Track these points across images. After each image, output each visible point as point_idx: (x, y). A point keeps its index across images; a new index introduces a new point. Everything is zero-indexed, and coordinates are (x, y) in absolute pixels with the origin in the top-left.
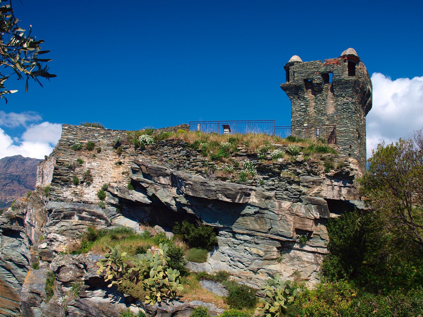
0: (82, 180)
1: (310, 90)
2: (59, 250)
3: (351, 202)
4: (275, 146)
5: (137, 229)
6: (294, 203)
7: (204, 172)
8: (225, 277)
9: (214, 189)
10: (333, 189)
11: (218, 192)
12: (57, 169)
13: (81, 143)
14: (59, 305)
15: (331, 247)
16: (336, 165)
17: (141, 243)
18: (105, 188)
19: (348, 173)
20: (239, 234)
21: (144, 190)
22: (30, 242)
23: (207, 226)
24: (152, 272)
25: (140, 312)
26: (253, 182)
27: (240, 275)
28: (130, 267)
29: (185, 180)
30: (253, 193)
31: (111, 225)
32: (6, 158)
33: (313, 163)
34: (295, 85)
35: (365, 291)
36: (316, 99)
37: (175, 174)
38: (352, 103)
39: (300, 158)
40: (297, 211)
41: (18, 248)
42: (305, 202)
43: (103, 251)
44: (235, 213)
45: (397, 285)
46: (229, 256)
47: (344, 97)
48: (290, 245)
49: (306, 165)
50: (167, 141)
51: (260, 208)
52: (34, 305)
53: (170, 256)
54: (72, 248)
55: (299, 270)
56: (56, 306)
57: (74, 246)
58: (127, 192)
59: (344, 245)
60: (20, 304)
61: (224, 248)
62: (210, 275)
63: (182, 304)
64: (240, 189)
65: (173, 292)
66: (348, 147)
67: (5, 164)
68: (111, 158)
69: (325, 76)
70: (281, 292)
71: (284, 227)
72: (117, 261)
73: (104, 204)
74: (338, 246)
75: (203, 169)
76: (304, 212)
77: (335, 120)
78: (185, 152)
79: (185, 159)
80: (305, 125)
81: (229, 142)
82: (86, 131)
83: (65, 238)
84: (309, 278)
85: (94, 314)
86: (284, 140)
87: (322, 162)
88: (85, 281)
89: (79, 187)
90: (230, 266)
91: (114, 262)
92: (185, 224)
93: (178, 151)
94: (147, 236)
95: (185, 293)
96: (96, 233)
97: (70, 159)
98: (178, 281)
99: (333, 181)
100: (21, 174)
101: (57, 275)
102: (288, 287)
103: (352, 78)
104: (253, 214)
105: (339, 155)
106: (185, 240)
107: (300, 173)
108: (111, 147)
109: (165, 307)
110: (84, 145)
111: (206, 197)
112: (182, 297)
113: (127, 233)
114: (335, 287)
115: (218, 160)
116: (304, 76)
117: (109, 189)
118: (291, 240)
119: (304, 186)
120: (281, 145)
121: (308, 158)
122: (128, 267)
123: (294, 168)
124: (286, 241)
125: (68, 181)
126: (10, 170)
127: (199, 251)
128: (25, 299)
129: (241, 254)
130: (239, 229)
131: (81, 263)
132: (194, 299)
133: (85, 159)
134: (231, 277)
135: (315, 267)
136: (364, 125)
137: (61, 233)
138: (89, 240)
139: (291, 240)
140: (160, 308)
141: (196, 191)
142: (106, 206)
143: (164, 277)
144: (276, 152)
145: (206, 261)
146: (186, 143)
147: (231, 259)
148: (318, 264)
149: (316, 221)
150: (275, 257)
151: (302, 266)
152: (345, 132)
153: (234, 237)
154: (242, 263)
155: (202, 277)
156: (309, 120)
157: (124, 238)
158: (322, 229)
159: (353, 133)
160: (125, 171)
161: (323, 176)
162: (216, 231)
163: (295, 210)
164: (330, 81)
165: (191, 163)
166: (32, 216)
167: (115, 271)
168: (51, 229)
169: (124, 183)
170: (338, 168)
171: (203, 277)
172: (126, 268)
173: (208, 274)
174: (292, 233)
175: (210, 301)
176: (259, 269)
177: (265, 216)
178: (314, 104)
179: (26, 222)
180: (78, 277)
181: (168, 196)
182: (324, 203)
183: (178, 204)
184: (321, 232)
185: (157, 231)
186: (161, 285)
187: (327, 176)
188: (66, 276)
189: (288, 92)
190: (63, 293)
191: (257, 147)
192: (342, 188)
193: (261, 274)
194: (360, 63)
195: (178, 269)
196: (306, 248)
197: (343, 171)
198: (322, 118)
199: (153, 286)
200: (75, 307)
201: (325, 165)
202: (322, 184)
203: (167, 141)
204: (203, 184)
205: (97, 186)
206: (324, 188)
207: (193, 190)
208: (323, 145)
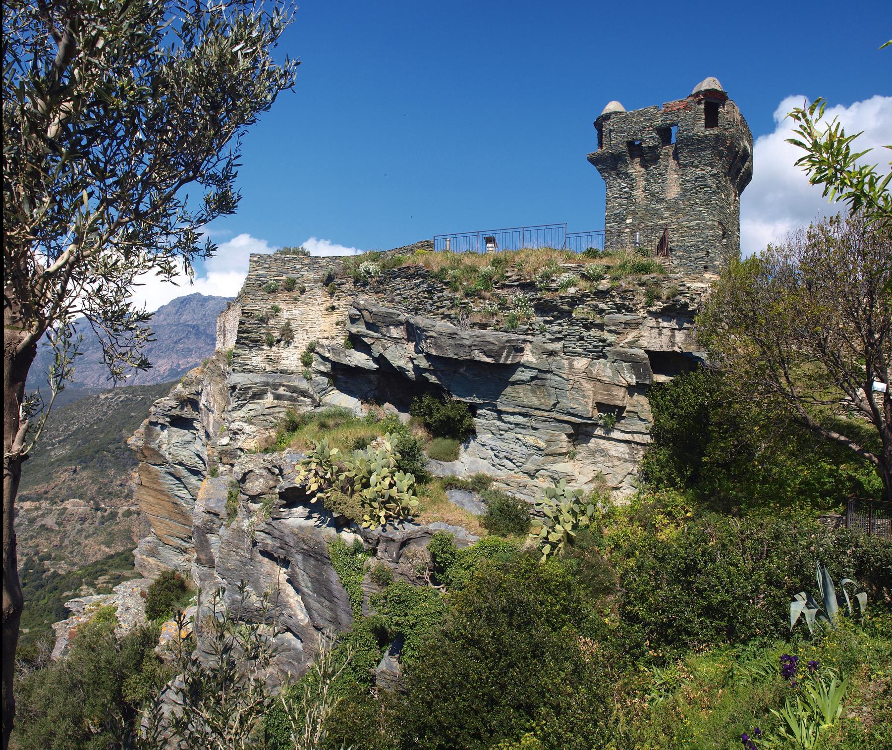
0: (279, 338)
1: (638, 160)
2: (246, 446)
3: (696, 354)
4: (563, 268)
5: (358, 409)
6: (594, 361)
7: (453, 316)
8: (484, 483)
9: (467, 342)
10: (660, 334)
11: (473, 348)
12: (244, 324)
13: (277, 281)
14: (243, 531)
15: (657, 433)
16: (665, 293)
17: (362, 433)
18: (312, 349)
19: (686, 305)
20: (508, 413)
21: (366, 349)
22: (208, 436)
23: (458, 402)
24: (373, 479)
25: (356, 540)
26: (528, 329)
27: (508, 482)
28: (343, 472)
29: (426, 331)
30: (528, 347)
31: (319, 405)
32: (179, 298)
33: (626, 291)
35: (708, 508)
36: (648, 174)
37: (411, 321)
38: (711, 176)
39: (604, 285)
40: (598, 373)
41: (191, 445)
42: (611, 358)
43: (307, 447)
44: (500, 380)
45: (766, 498)
46: (493, 450)
47: (697, 167)
48: (589, 429)
49: (614, 297)
50: (399, 269)
51: (540, 371)
52: (211, 531)
53: (402, 452)
54: (264, 443)
55: (604, 472)
56: (240, 532)
57: (266, 441)
58: (343, 352)
59: (677, 429)
60: (192, 529)
61: (484, 437)
62: (462, 482)
63: (416, 528)
64: (507, 342)
65: (404, 509)
66: (703, 253)
67: (176, 309)
68: (319, 300)
69: (664, 133)
70: (567, 509)
71: (577, 400)
72: (325, 461)
73: (309, 373)
74: (667, 431)
75: (453, 312)
76: (611, 374)
78: (425, 285)
79: (425, 298)
80: (628, 221)
81: (493, 265)
82: (283, 261)
83: (254, 428)
84: (620, 485)
85: (291, 544)
86: (580, 257)
87: (642, 290)
88: (279, 493)
89: (274, 349)
90: (494, 465)
91: (319, 464)
92: (426, 400)
93: (415, 284)
94: (372, 420)
95: (422, 510)
96: (298, 420)
97: (260, 307)
98: (411, 491)
99: (660, 320)
100: (200, 322)
101: (242, 485)
102: (577, 501)
103: (712, 132)
104: (529, 381)
105: (671, 275)
106: (427, 426)
107: (604, 311)
108: (320, 284)
109: (392, 533)
110: (281, 283)
111: (456, 357)
112: (417, 516)
113: (343, 416)
114: (659, 501)
115: (474, 296)
116: (628, 136)
117: (318, 349)
118: (589, 422)
119: (610, 331)
120: (573, 265)
121: (617, 283)
122: (341, 470)
123: (594, 302)
124: (582, 423)
125: (258, 341)
126: (184, 318)
127: (447, 442)
128: (198, 522)
129: (511, 446)
130: (507, 405)
131: (275, 467)
132: (435, 520)
133: (283, 306)
134: (495, 483)
135: (630, 467)
136: (737, 213)
137: (249, 421)
138: (288, 430)
139: (589, 422)
140: (383, 534)
141: (442, 348)
142: (313, 376)
143: (391, 486)
144: (565, 277)
145: (457, 459)
146: (427, 272)
147: (495, 455)
148: (635, 462)
149: (631, 390)
150: (564, 451)
151: (608, 464)
152: (699, 229)
153: (500, 419)
154: (511, 460)
155: (450, 484)
156: (634, 213)
157: (337, 425)
158: (642, 402)
159: (712, 229)
160: (340, 320)
161: (642, 313)
162: (473, 409)
163: (595, 373)
164: (673, 140)
165: (435, 302)
166: (211, 396)
167: (322, 477)
168: (235, 415)
169: (339, 338)
170: (668, 298)
171: (451, 484)
172: (337, 472)
173: (458, 480)
174: (591, 409)
175: (459, 523)
176: (538, 471)
177: (548, 383)
178: (644, 183)
179: (201, 405)
180: (271, 489)
181: (402, 356)
182: (644, 359)
183: (416, 368)
184: (640, 408)
185: (387, 412)
186: (386, 498)
187: (649, 312)
188: (255, 486)
189: (600, 166)
190: (250, 513)
191: (535, 271)
192: (676, 332)
193: (541, 479)
194: (728, 102)
195: (413, 472)
196: (616, 434)
197: (676, 303)
198: (659, 206)
199: (375, 500)
200: (266, 533)
201: (646, 294)
202: (641, 327)
203: (399, 269)
204: (452, 335)
205: (300, 346)
206: (645, 333)
207: (438, 346)
208: (645, 260)
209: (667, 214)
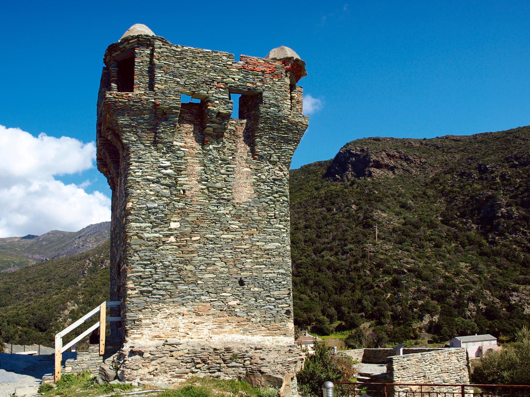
34: (155, 105)
36: (205, 155)
47: (274, 163)
77: (255, 221)
80: (173, 225)
115: (452, 140)
152: (279, 255)
198: (222, 210)
209: (235, 225)
